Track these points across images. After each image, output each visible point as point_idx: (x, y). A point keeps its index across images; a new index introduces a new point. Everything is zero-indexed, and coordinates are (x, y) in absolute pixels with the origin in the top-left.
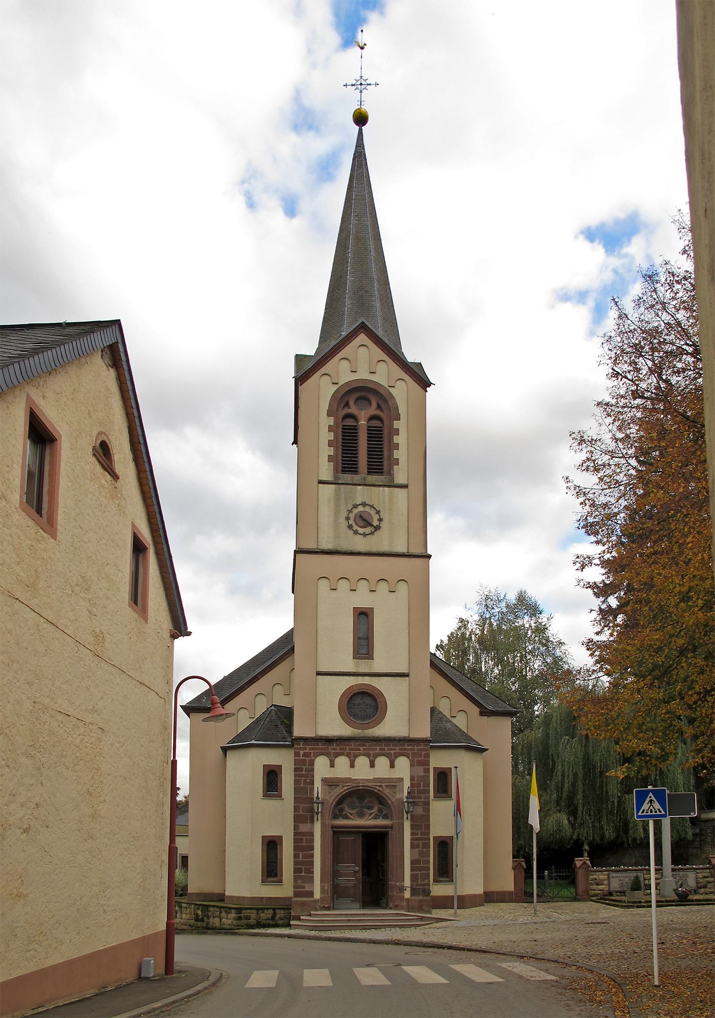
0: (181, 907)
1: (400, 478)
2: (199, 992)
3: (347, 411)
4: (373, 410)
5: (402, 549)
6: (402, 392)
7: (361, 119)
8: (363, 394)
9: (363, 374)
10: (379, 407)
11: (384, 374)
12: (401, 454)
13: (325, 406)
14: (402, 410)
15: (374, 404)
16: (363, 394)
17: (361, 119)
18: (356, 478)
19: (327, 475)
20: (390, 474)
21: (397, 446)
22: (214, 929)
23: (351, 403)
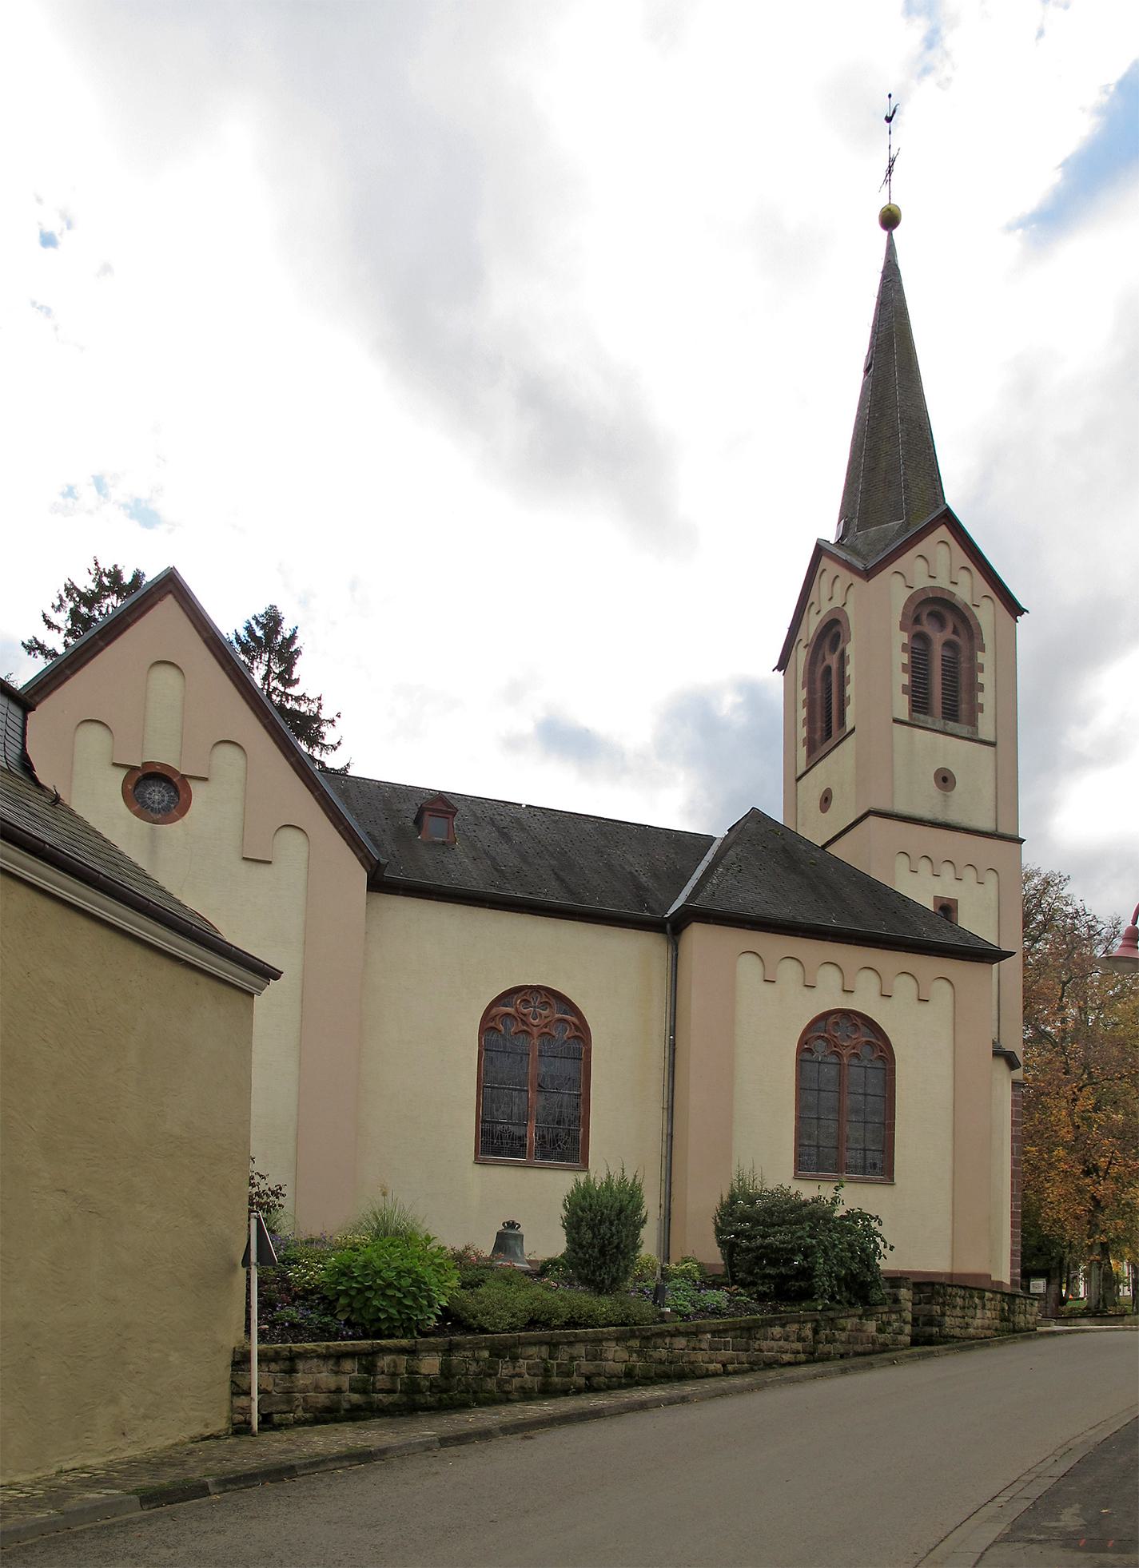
0: (982, 1298)
1: (986, 729)
2: (485, 1435)
3: (918, 628)
4: (948, 634)
5: (987, 825)
6: (987, 614)
7: (890, 220)
8: (937, 608)
9: (942, 582)
10: (955, 632)
11: (967, 589)
12: (985, 698)
13: (897, 617)
14: (987, 639)
15: (950, 628)
16: (937, 608)
17: (890, 220)
18: (928, 721)
19: (903, 712)
20: (973, 722)
21: (981, 688)
22: (1021, 1331)
23: (924, 617)
